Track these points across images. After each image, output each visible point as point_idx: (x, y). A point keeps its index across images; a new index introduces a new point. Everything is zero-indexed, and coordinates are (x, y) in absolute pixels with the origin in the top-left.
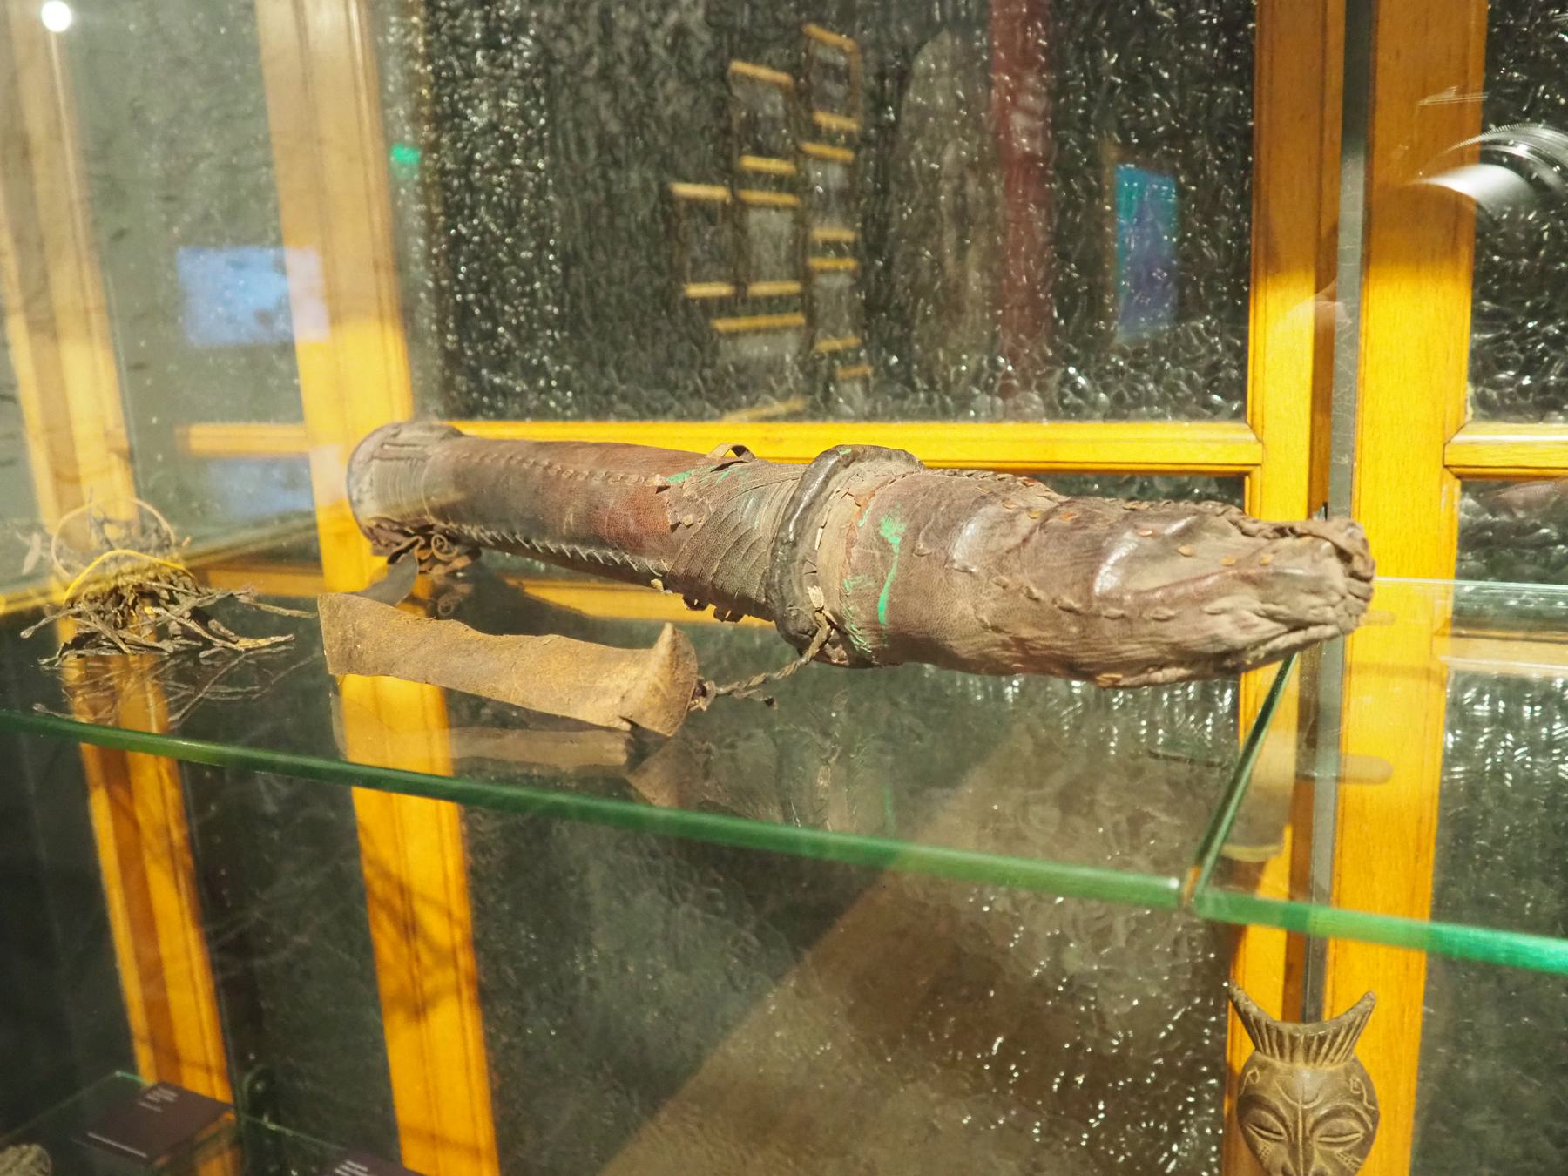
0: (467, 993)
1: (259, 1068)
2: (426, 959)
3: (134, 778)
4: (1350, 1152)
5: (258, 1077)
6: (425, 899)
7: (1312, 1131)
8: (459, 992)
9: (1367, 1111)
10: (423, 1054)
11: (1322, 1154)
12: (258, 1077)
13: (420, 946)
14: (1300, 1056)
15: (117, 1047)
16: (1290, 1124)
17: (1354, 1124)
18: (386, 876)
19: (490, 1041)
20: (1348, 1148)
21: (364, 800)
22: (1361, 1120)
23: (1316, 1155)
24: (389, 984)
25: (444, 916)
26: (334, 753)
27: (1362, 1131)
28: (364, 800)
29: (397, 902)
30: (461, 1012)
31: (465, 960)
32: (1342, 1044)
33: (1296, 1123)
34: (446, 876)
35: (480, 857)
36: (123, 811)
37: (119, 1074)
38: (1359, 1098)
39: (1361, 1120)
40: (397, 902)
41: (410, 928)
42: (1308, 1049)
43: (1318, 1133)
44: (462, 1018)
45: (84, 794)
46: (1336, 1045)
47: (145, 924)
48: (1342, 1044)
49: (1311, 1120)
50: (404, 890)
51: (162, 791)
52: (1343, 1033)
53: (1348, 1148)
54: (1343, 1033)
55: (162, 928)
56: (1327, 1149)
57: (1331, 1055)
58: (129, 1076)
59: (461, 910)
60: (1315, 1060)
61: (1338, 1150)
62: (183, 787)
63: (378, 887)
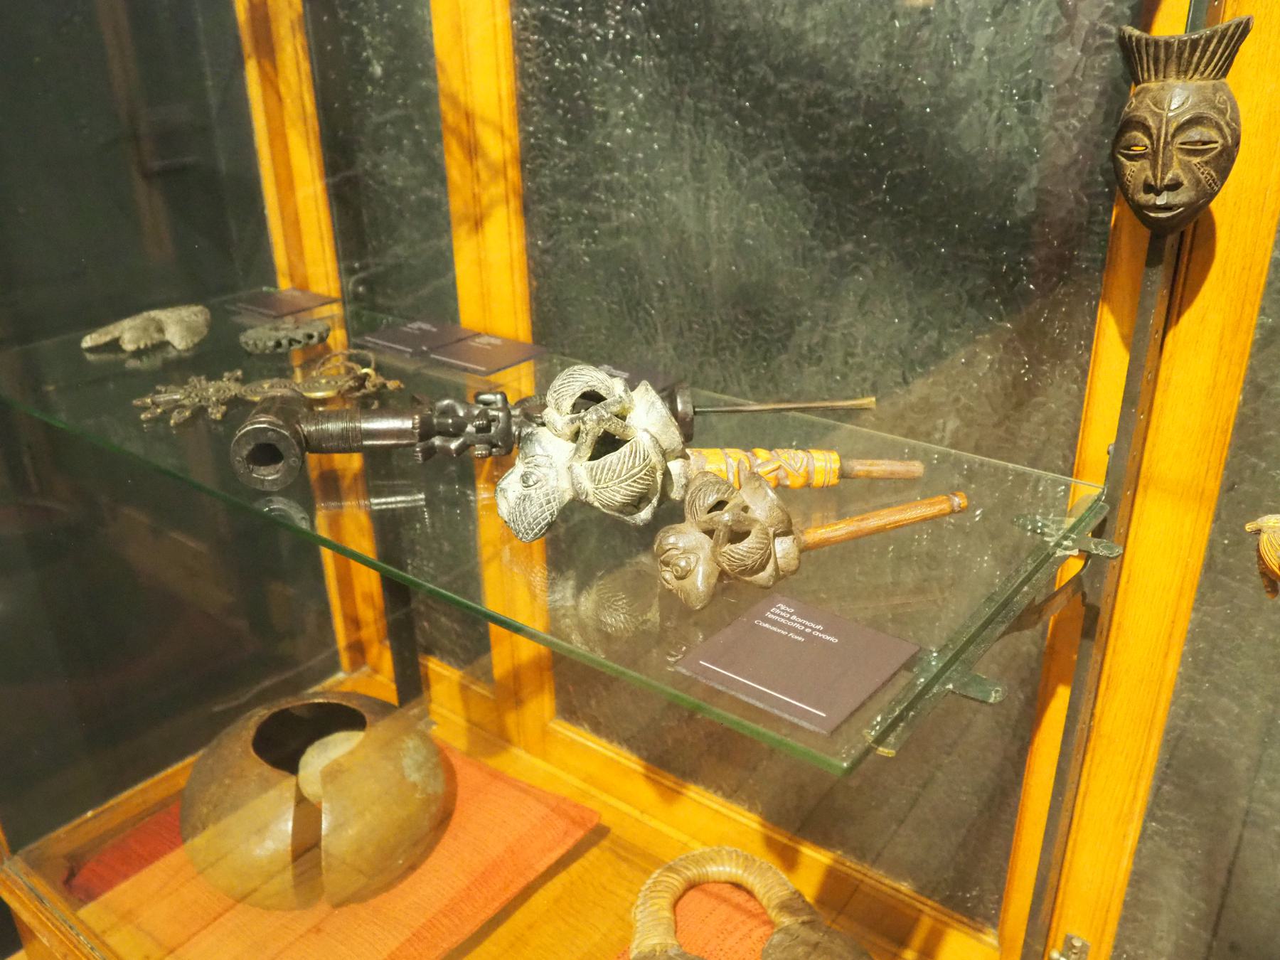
0: (515, 204)
1: (361, 275)
2: (484, 175)
3: (278, 56)
4: (1207, 163)
5: (359, 283)
6: (485, 122)
7: (1174, 136)
8: (507, 202)
9: (1228, 125)
10: (480, 264)
11: (1180, 161)
12: (359, 283)
13: (480, 164)
14: (1173, 68)
15: (269, 275)
16: (1154, 131)
17: (1214, 134)
18: (454, 101)
19: (530, 248)
20: (1206, 158)
21: (494, 629)
22: (1220, 129)
23: (1175, 164)
24: (457, 204)
25: (499, 142)
26: (477, 594)
27: (1221, 141)
28: (494, 629)
29: (464, 127)
30: (509, 219)
31: (513, 173)
32: (1214, 53)
33: (1159, 129)
34: (500, 97)
35: (526, 81)
36: (270, 81)
37: (265, 289)
38: (1222, 112)
39: (1220, 129)
40: (464, 127)
41: (472, 150)
42: (1180, 57)
43: (1179, 139)
44: (509, 225)
45: (239, 63)
46: (1208, 54)
47: (286, 184)
48: (1214, 53)
49: (1174, 125)
50: (469, 117)
51: (298, 63)
52: (1215, 41)
53: (1206, 158)
54: (1215, 41)
55: (298, 182)
56: (1187, 158)
57: (1201, 68)
58: (272, 290)
59: (512, 130)
60: (1186, 72)
61: (1196, 160)
62: (312, 63)
63: (450, 116)
